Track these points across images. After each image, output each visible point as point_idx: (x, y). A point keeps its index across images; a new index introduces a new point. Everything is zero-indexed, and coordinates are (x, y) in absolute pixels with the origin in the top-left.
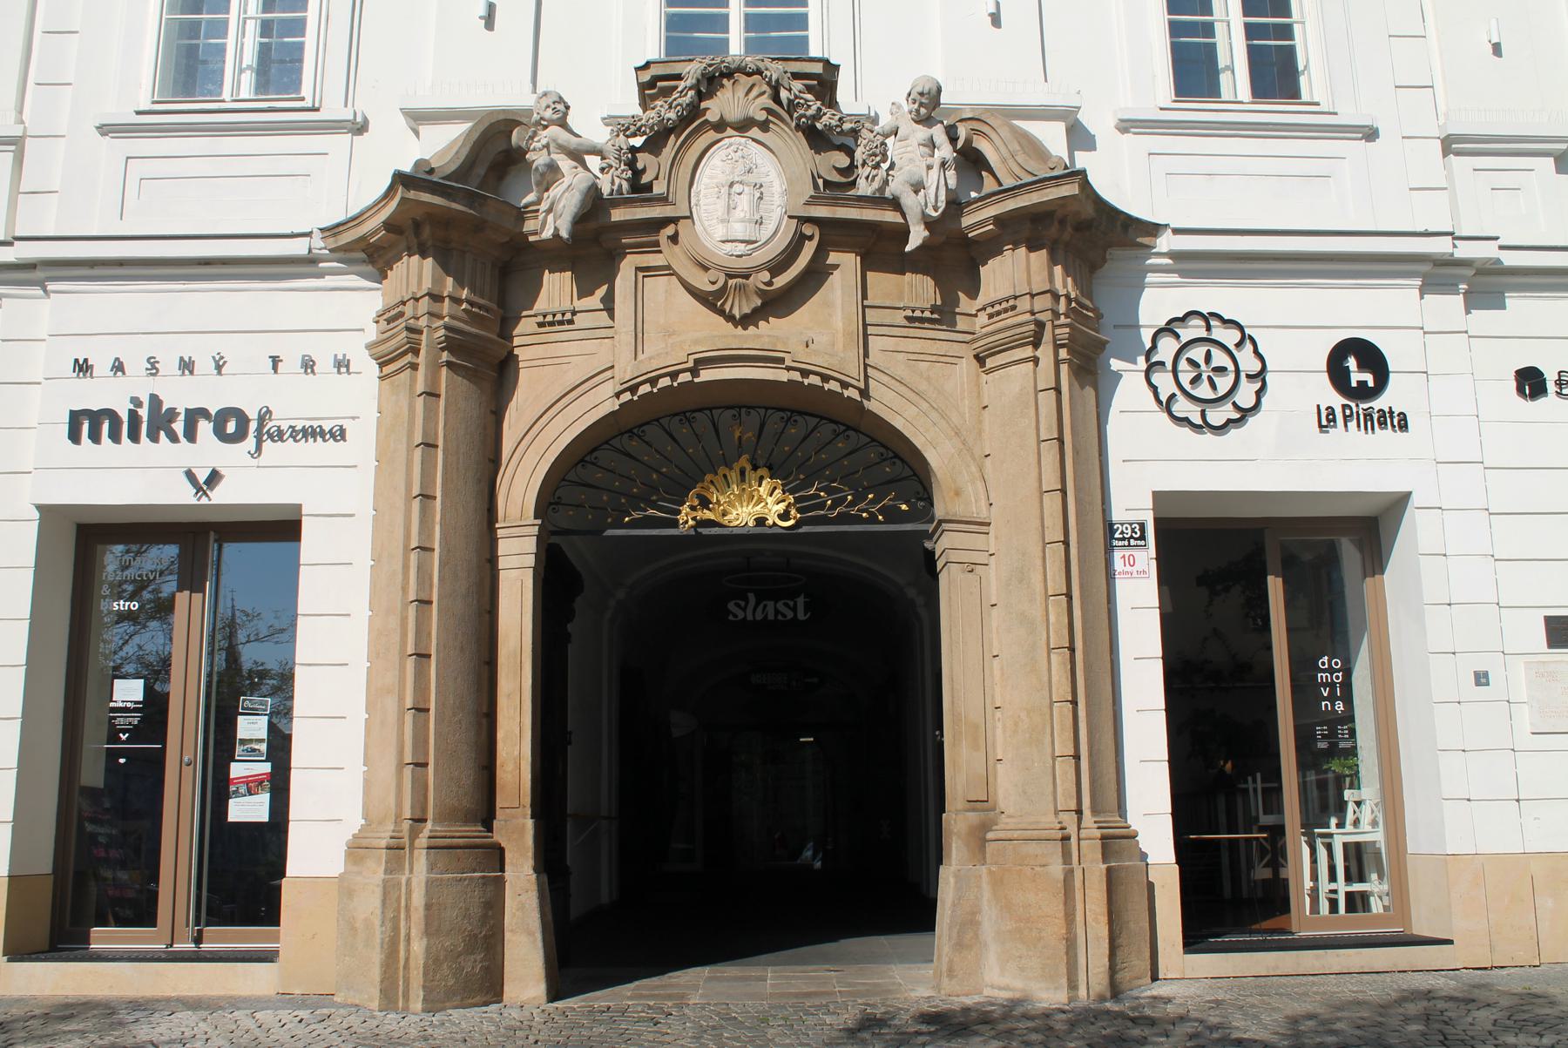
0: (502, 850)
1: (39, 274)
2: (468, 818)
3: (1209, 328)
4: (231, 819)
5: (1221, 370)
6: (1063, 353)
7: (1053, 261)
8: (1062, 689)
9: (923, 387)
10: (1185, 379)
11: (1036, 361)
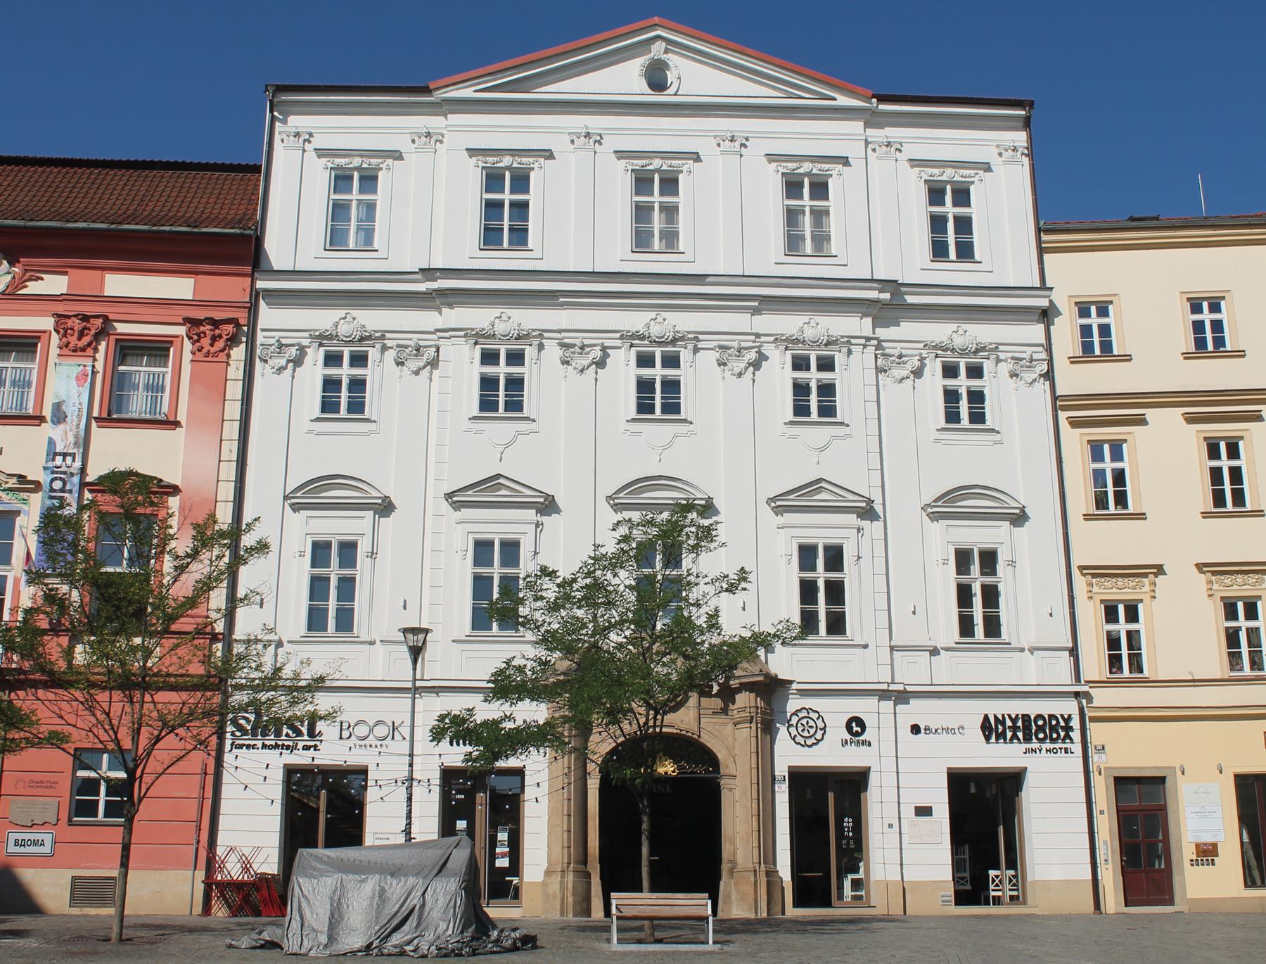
0: (590, 874)
1: (436, 690)
2: (581, 864)
3: (808, 713)
4: (497, 866)
5: (811, 727)
6: (759, 725)
7: (757, 696)
8: (755, 827)
9: (716, 734)
10: (800, 729)
11: (751, 728)
